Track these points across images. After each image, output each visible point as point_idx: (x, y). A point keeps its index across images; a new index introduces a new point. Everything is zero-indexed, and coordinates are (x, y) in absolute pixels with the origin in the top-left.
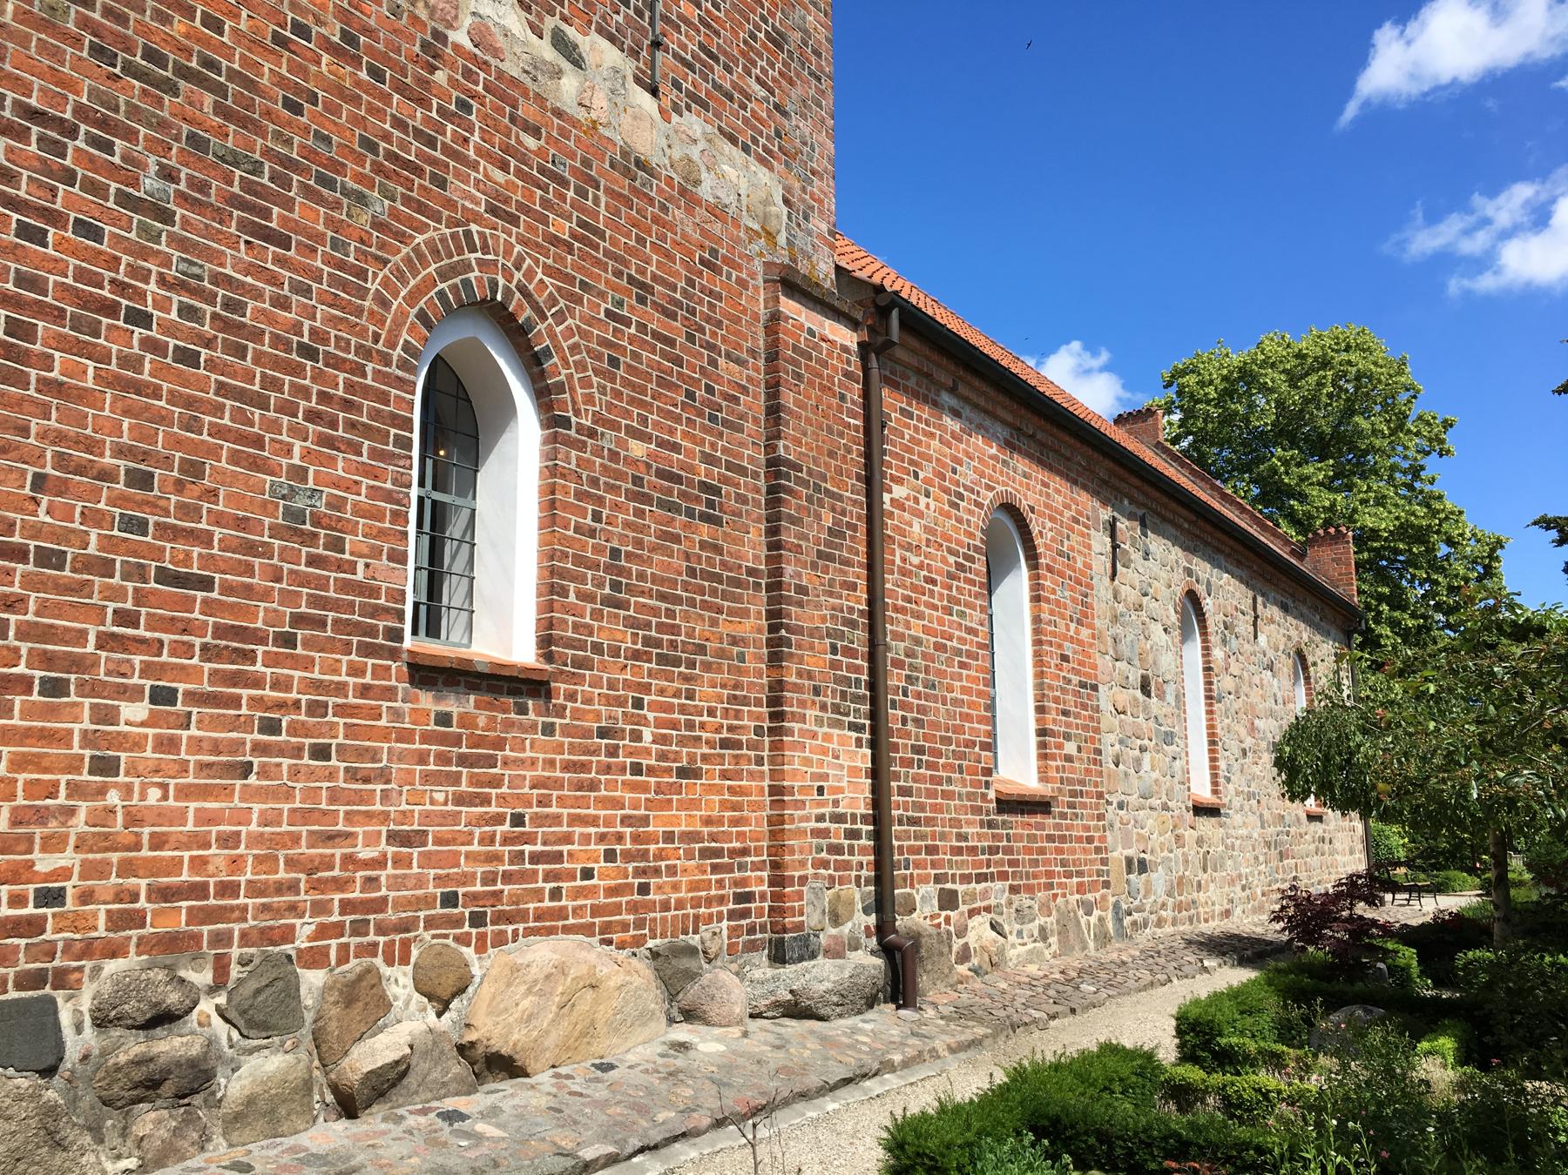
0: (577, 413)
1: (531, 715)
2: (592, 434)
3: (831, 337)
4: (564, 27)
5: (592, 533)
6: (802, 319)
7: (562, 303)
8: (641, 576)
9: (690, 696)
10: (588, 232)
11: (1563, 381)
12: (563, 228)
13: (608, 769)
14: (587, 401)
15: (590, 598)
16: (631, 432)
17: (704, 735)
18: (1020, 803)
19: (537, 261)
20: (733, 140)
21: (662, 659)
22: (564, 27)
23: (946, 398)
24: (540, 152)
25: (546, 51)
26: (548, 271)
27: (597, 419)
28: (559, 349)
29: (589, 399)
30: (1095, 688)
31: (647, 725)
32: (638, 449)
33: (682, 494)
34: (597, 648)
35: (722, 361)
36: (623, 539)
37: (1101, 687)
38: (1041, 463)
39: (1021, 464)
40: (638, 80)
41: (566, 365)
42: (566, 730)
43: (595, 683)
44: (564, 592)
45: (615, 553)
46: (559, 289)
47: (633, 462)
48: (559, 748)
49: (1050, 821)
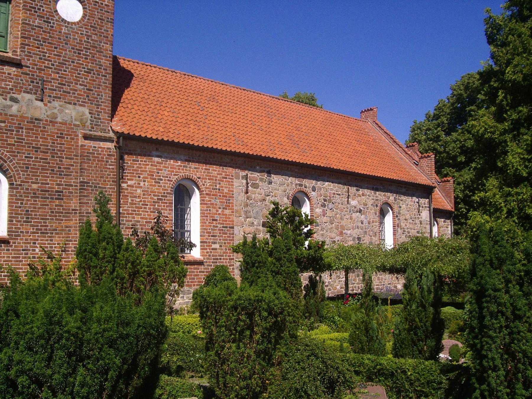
0: (16, 181)
1: (3, 247)
2: (20, 185)
3: (103, 147)
4: (13, 95)
5: (20, 207)
6: (91, 144)
7: (12, 158)
8: (36, 215)
9: (52, 240)
10: (20, 140)
11: (77, 2)
12: (11, 141)
13: (25, 258)
14: (203, 188)
15: (20, 221)
16: (33, 183)
17: (56, 249)
18: (194, 262)
19: (4, 151)
20: (70, 103)
21: (42, 233)
22: (13, 95)
23: (154, 153)
24: (6, 126)
25: (9, 103)
26: (8, 152)
27: (22, 182)
28: (11, 168)
29: (20, 178)
30: (233, 228)
31: (37, 248)
32: (35, 186)
33: (49, 195)
34: (22, 232)
35: (64, 160)
36: (30, 207)
37: (235, 227)
38: (206, 163)
39: (193, 165)
40: (36, 100)
41: (13, 171)
42: (13, 250)
43: (22, 239)
44: (12, 221)
45: (27, 211)
46: (11, 155)
47: (34, 190)
48: (11, 254)
49: (203, 267)
